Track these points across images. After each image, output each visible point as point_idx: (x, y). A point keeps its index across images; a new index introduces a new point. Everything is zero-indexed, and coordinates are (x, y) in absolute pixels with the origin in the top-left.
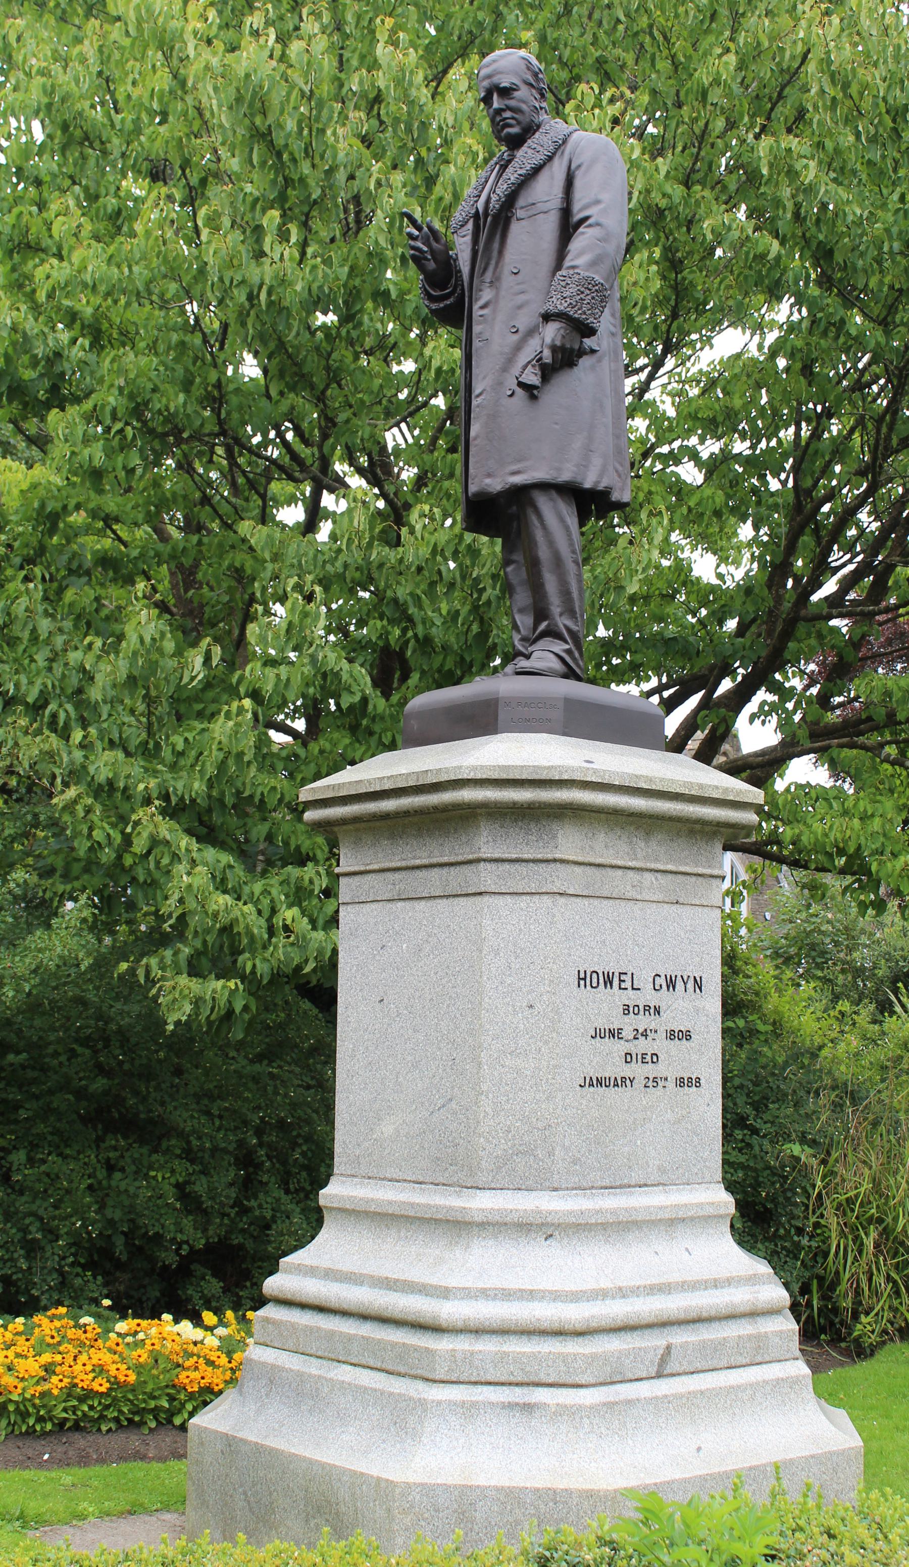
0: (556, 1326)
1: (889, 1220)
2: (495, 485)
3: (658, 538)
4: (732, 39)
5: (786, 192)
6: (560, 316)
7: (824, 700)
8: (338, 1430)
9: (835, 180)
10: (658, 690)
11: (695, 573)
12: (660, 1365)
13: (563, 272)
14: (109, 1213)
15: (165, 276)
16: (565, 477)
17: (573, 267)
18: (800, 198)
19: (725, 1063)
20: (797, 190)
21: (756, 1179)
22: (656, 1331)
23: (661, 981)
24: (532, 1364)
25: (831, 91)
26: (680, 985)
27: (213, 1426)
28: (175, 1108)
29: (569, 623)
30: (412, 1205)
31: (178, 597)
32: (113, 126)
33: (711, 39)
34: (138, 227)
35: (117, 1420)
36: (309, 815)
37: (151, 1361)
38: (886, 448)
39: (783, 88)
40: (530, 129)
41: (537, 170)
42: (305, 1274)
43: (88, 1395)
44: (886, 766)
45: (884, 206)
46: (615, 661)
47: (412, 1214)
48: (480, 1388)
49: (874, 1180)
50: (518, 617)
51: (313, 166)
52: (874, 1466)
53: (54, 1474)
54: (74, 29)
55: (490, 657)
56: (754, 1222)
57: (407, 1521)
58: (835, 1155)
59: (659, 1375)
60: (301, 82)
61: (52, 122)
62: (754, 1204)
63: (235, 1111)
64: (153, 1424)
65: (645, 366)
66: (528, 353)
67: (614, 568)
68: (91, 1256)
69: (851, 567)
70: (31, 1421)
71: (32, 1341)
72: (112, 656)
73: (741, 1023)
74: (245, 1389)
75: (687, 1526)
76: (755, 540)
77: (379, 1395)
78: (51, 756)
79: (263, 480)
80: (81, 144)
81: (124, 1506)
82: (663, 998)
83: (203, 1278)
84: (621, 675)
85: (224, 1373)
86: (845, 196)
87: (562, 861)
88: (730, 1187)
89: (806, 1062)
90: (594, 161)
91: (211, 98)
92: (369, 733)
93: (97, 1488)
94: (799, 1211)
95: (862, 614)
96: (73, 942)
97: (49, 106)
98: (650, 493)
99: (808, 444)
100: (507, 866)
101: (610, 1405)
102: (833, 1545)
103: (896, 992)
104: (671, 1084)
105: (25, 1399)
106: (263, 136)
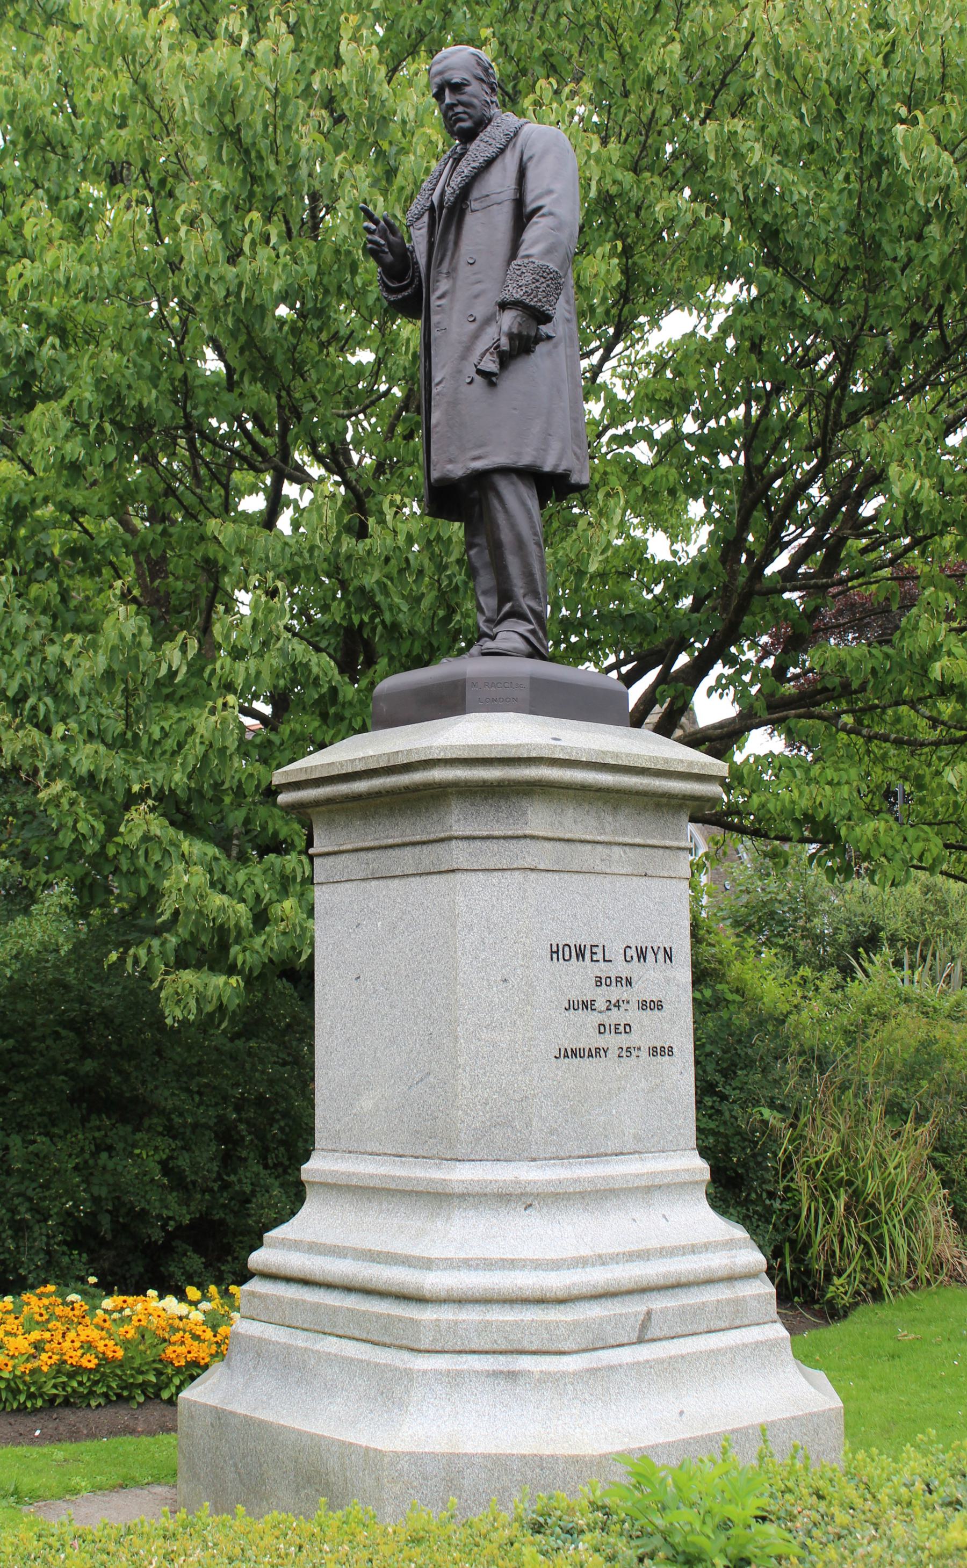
0: (538, 1294)
1: (859, 1182)
2: (457, 470)
3: (617, 519)
4: (677, 29)
5: (733, 175)
6: (516, 304)
7: (779, 672)
8: (326, 1401)
9: (779, 162)
10: (616, 666)
11: (651, 551)
12: (641, 1331)
13: (518, 261)
14: (96, 1191)
15: (134, 275)
16: (525, 460)
17: (528, 256)
18: (747, 180)
19: (695, 1030)
20: (744, 172)
21: (727, 1144)
22: (636, 1297)
23: (632, 952)
24: (517, 1331)
25: (775, 75)
26: (650, 956)
27: (202, 1400)
28: (156, 1087)
29: (533, 604)
30: (393, 1178)
31: (145, 589)
32: (74, 131)
33: (657, 29)
34: (99, 228)
35: (106, 1395)
36: (282, 798)
37: (138, 1336)
38: (835, 423)
39: (726, 75)
40: (482, 123)
41: (490, 163)
42: (289, 1248)
43: (78, 1370)
44: (842, 735)
45: (829, 187)
46: (574, 639)
47: (393, 1187)
48: (465, 1357)
49: (844, 1145)
50: (482, 600)
51: (277, 162)
52: (855, 1424)
53: (45, 1450)
54: (33, 37)
55: (455, 640)
56: (725, 1187)
57: (397, 1489)
58: (803, 1120)
59: (640, 1341)
60: (267, 81)
61: (14, 129)
62: (726, 1169)
63: (215, 1088)
64: (141, 1399)
65: (597, 349)
66: (485, 341)
67: (575, 550)
68: (76, 1235)
69: (802, 541)
70: (22, 1398)
71: (21, 1319)
72: (91, 652)
73: (708, 993)
74: (233, 1363)
75: (679, 1489)
76: (708, 518)
77: (364, 1365)
78: (34, 750)
79: (225, 471)
80: (43, 149)
81: (117, 1481)
82: (634, 969)
83: (185, 1254)
84: (576, 655)
85: (209, 1347)
86: (790, 177)
87: (533, 837)
88: (704, 1152)
89: (770, 1028)
90: (545, 152)
91: (185, 102)
92: (337, 719)
93: (88, 1464)
94: (769, 1176)
95: (816, 586)
96: (51, 928)
97: (12, 114)
98: (605, 473)
99: (758, 422)
100: (478, 843)
101: (593, 1371)
102: (822, 1506)
103: (857, 957)
104: (644, 1054)
105: (15, 1376)
106: (232, 134)
